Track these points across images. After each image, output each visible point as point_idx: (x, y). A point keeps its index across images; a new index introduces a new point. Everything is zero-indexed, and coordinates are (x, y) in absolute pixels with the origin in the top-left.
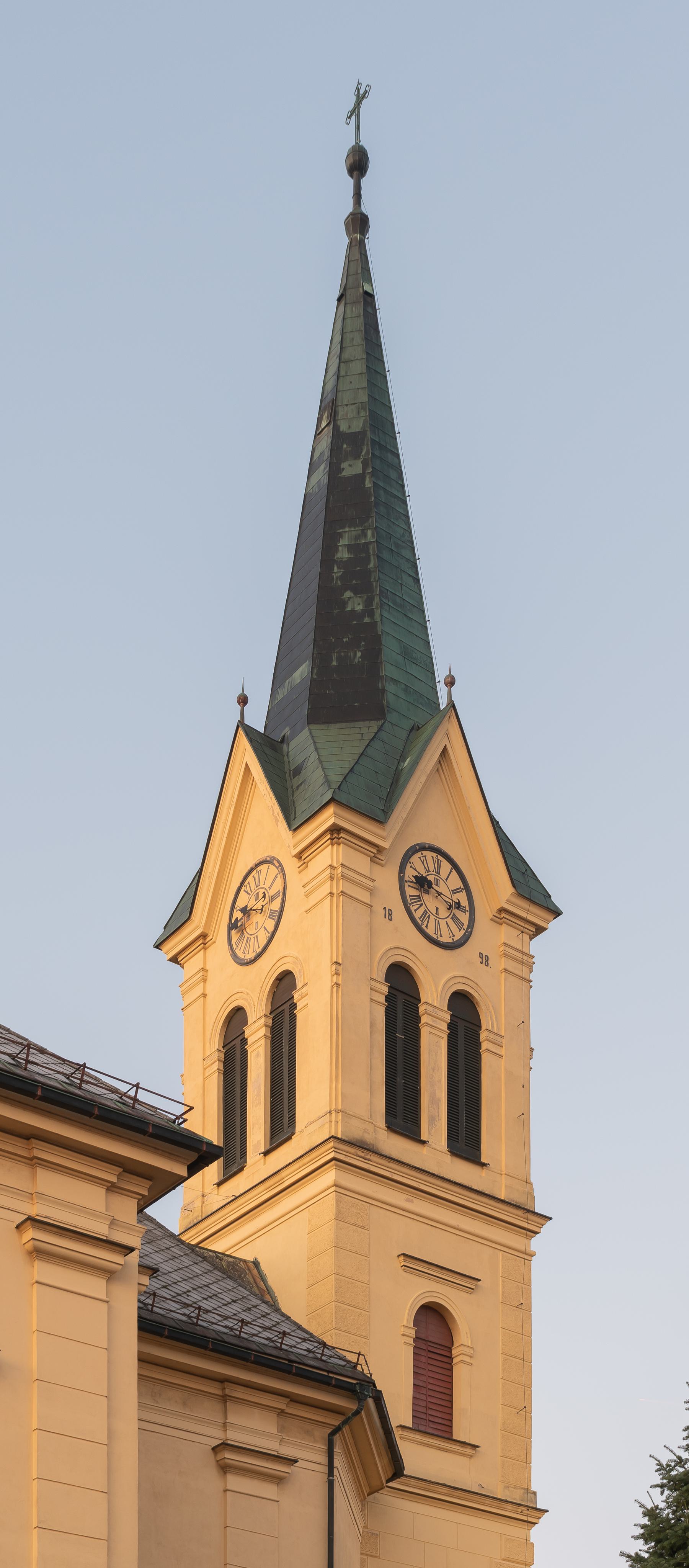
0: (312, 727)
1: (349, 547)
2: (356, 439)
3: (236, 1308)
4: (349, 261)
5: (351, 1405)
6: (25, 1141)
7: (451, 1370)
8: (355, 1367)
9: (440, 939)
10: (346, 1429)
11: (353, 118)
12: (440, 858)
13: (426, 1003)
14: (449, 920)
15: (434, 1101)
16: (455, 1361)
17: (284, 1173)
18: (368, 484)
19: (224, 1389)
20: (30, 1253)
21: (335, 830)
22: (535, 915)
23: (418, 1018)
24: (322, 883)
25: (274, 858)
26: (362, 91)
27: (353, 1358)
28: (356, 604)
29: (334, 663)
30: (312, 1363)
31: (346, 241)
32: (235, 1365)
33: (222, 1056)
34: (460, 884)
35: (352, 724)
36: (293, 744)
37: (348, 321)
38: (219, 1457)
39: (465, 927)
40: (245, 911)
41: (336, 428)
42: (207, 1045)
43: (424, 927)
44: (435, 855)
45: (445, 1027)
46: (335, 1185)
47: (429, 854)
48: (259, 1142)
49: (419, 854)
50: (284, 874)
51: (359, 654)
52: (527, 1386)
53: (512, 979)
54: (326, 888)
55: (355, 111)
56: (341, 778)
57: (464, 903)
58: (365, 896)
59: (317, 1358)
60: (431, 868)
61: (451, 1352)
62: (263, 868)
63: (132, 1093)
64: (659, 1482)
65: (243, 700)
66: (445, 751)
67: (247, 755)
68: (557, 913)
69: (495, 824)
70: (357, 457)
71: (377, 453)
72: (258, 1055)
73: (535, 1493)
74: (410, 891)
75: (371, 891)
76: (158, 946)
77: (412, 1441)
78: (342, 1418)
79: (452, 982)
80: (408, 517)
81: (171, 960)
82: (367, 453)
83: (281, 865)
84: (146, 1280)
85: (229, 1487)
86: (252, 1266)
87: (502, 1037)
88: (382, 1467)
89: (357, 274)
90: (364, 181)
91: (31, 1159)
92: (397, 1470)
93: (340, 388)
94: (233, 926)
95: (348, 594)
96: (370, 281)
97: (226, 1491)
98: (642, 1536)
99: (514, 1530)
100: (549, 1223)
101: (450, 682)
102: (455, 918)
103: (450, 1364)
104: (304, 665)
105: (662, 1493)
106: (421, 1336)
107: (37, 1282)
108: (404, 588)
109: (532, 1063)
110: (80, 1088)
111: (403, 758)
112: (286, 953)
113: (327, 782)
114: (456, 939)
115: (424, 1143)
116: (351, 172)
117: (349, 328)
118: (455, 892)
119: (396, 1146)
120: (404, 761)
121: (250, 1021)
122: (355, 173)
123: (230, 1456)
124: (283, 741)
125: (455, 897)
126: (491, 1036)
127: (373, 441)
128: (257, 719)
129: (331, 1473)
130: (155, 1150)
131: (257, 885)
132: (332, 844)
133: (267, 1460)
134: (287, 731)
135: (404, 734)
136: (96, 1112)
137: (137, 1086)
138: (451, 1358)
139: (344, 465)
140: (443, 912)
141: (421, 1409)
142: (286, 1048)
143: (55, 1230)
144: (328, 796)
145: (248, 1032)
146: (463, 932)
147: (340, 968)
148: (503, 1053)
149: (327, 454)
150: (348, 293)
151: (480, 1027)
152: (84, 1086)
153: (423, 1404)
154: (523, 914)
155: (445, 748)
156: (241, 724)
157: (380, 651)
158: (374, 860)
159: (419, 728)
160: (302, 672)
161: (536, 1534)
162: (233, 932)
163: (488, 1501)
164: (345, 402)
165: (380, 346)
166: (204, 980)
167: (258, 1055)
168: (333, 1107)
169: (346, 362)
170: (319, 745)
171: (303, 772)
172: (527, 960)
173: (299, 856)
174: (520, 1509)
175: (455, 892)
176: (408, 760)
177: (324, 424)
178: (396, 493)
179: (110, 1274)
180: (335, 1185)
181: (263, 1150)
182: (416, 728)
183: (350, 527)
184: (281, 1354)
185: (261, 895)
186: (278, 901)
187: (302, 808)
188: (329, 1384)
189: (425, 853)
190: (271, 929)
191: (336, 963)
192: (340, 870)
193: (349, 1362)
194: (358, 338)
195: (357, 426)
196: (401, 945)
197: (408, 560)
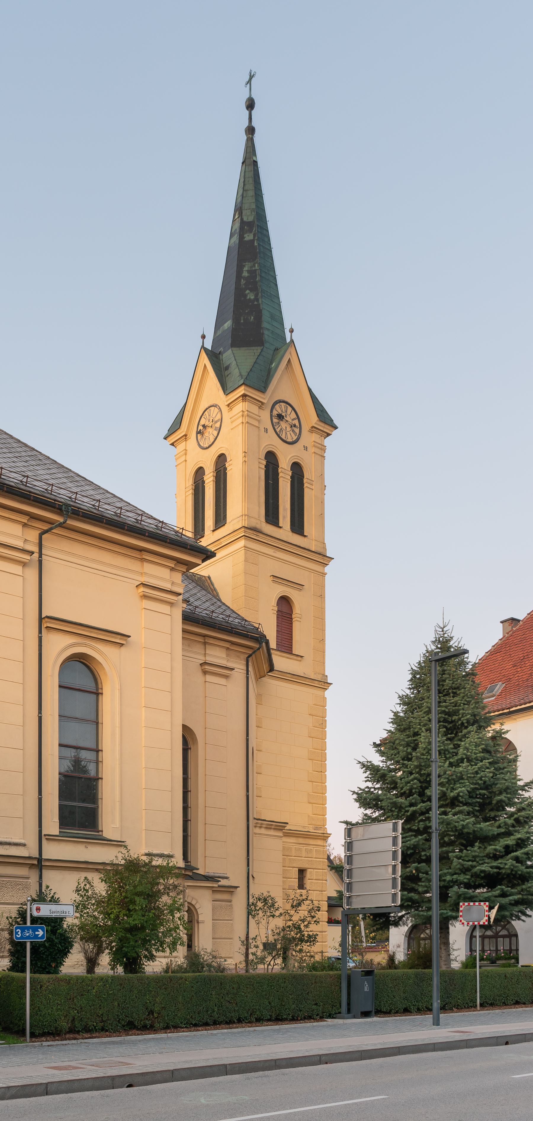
0: (234, 349)
1: (248, 271)
2: (250, 224)
3: (208, 604)
4: (247, 144)
5: (256, 645)
7: (292, 624)
9: (287, 440)
10: (253, 656)
12: (287, 405)
13: (282, 468)
14: (291, 432)
15: (285, 509)
16: (293, 620)
17: (222, 540)
18: (256, 244)
19: (205, 639)
20: (141, 597)
21: (244, 396)
22: (327, 429)
23: (278, 474)
24: (238, 418)
26: (252, 74)
27: (257, 626)
28: (251, 296)
30: (241, 628)
31: (245, 138)
32: (210, 630)
33: (194, 487)
34: (295, 416)
35: (250, 348)
36: (224, 355)
37: (247, 173)
38: (203, 667)
39: (298, 434)
40: (204, 426)
42: (187, 482)
44: (285, 404)
45: (289, 478)
46: (245, 547)
47: (283, 404)
49: (278, 404)
50: (221, 412)
51: (252, 318)
52: (323, 630)
53: (317, 456)
54: (240, 420)
55: (249, 82)
56: (247, 374)
57: (297, 424)
58: (256, 423)
59: (242, 626)
60: (284, 410)
61: (292, 616)
62: (212, 408)
63: (181, 531)
64: (399, 702)
65: (203, 337)
66: (289, 361)
67: (205, 360)
68: (336, 428)
69: (310, 390)
70: (251, 232)
71: (259, 230)
72: (210, 488)
73: (327, 676)
74: (275, 420)
75: (259, 421)
76: (165, 438)
77: (276, 655)
78: (253, 651)
80: (272, 258)
81: (171, 444)
82: (255, 230)
83: (220, 408)
84: (185, 605)
86: (207, 578)
87: (313, 481)
88: (266, 667)
89: (250, 152)
90: (253, 112)
91: (142, 559)
92: (271, 669)
93: (244, 202)
94: (199, 432)
95: (248, 292)
96: (256, 156)
97: (205, 682)
98: (392, 722)
99: (318, 692)
100: (333, 560)
101: (292, 331)
102: (293, 431)
103: (292, 621)
105: (400, 706)
106: (280, 610)
108: (271, 289)
109: (325, 492)
110: (161, 530)
111: (271, 363)
112: (222, 446)
113: (241, 375)
114: (294, 440)
117: (247, 176)
118: (293, 420)
119: (269, 529)
120: (272, 364)
121: (206, 474)
122: (249, 109)
123: (207, 667)
124: (220, 353)
125: (294, 422)
126: (309, 481)
127: (258, 225)
128: (209, 345)
129: (247, 673)
130: (190, 554)
131: (209, 416)
132: (243, 401)
133: (222, 669)
134: (221, 349)
135: (272, 352)
136: (168, 541)
137: (183, 529)
138: (292, 619)
139: (246, 235)
140: (289, 429)
141: (279, 641)
142: (222, 486)
144: (242, 382)
145: (205, 478)
146: (297, 437)
147: (246, 454)
148: (313, 488)
149: (238, 231)
150: (247, 161)
151: (304, 477)
152: (163, 529)
153: (280, 638)
154: (322, 429)
155: (289, 359)
156: (203, 347)
157: (261, 316)
158: (260, 408)
159: (278, 349)
161: (327, 693)
162: (198, 435)
163: (307, 680)
164: (246, 208)
165: (260, 184)
166: (186, 454)
168: (244, 514)
169: (247, 191)
170: (236, 358)
171: (230, 369)
172: (323, 448)
173: (228, 405)
174: (321, 683)
175: (293, 420)
176: (274, 364)
177: (237, 217)
178: (266, 247)
179: (171, 604)
180: (245, 547)
181: (212, 529)
182: (277, 349)
183: (248, 262)
184: (228, 625)
185: (211, 420)
186: (219, 423)
187: (230, 385)
188: (247, 637)
189: (281, 404)
190: (216, 435)
191: (245, 452)
192: (246, 413)
193: (255, 627)
194: (251, 181)
195: (251, 219)
196: (271, 444)
197: (272, 276)
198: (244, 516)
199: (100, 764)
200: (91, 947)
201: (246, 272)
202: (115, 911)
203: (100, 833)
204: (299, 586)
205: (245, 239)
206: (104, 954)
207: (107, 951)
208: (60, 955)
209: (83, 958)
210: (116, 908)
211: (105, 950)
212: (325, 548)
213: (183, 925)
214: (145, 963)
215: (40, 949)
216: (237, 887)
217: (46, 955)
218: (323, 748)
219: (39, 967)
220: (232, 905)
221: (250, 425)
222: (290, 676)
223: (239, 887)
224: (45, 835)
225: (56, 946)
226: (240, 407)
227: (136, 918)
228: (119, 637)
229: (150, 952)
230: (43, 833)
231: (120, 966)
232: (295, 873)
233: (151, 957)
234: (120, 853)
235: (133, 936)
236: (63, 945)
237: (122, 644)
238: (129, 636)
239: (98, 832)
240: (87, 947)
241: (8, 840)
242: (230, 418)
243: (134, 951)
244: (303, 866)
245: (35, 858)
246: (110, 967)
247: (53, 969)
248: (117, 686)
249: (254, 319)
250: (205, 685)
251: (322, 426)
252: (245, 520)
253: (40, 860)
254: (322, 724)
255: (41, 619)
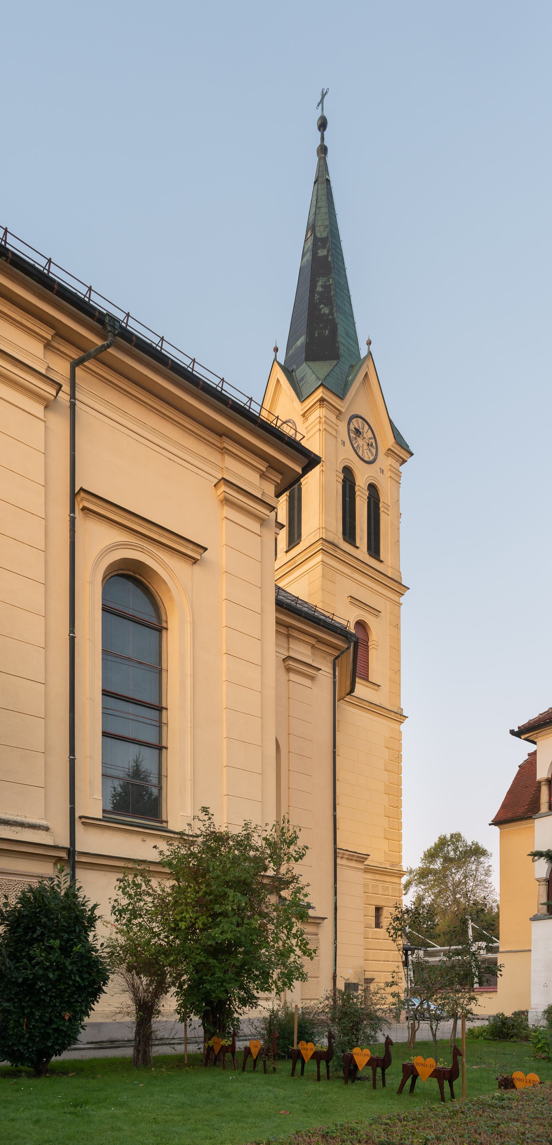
0: (307, 362)
1: (322, 286)
2: (324, 241)
4: (319, 166)
5: (344, 645)
6: (219, 437)
7: (368, 652)
8: (346, 628)
11: (320, 105)
14: (368, 450)
15: (362, 530)
16: (370, 648)
18: (330, 259)
19: (288, 631)
20: (222, 501)
21: (322, 400)
22: (403, 454)
24: (315, 426)
25: (290, 419)
26: (324, 92)
28: (326, 310)
29: (316, 335)
31: (317, 159)
34: (372, 436)
36: (297, 371)
37: (319, 191)
38: (286, 664)
39: (374, 455)
41: (315, 236)
43: (358, 451)
46: (322, 561)
47: (360, 420)
48: (283, 548)
51: (327, 332)
54: (317, 427)
55: (322, 102)
56: (324, 377)
57: (374, 445)
58: (334, 433)
60: (361, 426)
65: (276, 350)
67: (279, 374)
70: (325, 248)
71: (333, 247)
72: (283, 509)
74: (352, 435)
75: (336, 431)
79: (369, 479)
83: (294, 422)
85: (290, 679)
87: (389, 506)
90: (326, 133)
91: (222, 449)
93: (317, 219)
95: (322, 306)
96: (328, 175)
97: (289, 680)
99: (393, 725)
100: (408, 591)
101: (369, 343)
102: (370, 450)
103: (368, 649)
104: (302, 338)
107: (226, 518)
109: (401, 520)
111: (348, 376)
115: (357, 548)
116: (319, 129)
118: (370, 438)
119: (347, 547)
122: (321, 129)
124: (293, 371)
126: (385, 505)
132: (320, 407)
133: (308, 667)
134: (294, 367)
138: (368, 646)
139: (319, 251)
140: (365, 447)
142: (296, 504)
143: (236, 488)
144: (320, 383)
146: (373, 457)
149: (311, 248)
150: (319, 179)
154: (398, 453)
155: (367, 372)
156: (275, 359)
157: (337, 330)
158: (337, 417)
160: (301, 341)
161: (403, 727)
163: (384, 710)
164: (319, 225)
167: (283, 509)
168: (321, 526)
169: (319, 208)
172: (399, 474)
173: (303, 415)
177: (309, 235)
180: (322, 561)
182: (352, 366)
183: (322, 277)
187: (305, 393)
192: (324, 419)
194: (324, 198)
195: (324, 235)
197: (347, 295)
198: (321, 529)
199: (164, 728)
200: (144, 983)
201: (320, 287)
202: (188, 916)
203: (164, 825)
204: (376, 612)
205: (319, 255)
206: (169, 995)
207: (173, 989)
208: (80, 996)
209: (130, 1002)
210: (190, 911)
211: (170, 987)
212: (401, 578)
213: (300, 947)
214: (240, 1011)
215: (36, 983)
216: (324, 919)
217: (51, 997)
218: (399, 784)
219: (37, 1021)
220: (318, 939)
221: (327, 433)
222: (367, 704)
223: (326, 918)
224: (80, 817)
225: (70, 979)
226: (319, 412)
227: (226, 928)
228: (191, 546)
229: (247, 991)
230: (77, 814)
231: (195, 1014)
232: (373, 913)
233: (249, 1000)
234: (196, 820)
235: (220, 963)
236: (86, 976)
237: (195, 561)
238: (205, 549)
239: (162, 822)
240: (137, 981)
241: (19, 819)
242: (306, 428)
243: (222, 989)
244: (380, 904)
245: (63, 848)
246: (179, 1016)
247: (67, 1024)
248: (189, 618)
249: (328, 333)
250: (289, 684)
251: (398, 450)
252: (323, 533)
253: (71, 851)
254: (398, 758)
255: (73, 495)
